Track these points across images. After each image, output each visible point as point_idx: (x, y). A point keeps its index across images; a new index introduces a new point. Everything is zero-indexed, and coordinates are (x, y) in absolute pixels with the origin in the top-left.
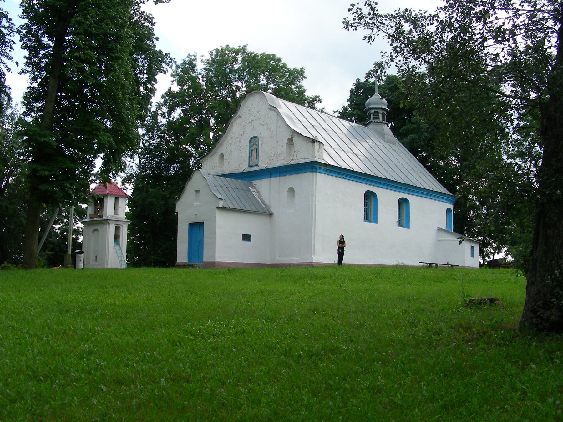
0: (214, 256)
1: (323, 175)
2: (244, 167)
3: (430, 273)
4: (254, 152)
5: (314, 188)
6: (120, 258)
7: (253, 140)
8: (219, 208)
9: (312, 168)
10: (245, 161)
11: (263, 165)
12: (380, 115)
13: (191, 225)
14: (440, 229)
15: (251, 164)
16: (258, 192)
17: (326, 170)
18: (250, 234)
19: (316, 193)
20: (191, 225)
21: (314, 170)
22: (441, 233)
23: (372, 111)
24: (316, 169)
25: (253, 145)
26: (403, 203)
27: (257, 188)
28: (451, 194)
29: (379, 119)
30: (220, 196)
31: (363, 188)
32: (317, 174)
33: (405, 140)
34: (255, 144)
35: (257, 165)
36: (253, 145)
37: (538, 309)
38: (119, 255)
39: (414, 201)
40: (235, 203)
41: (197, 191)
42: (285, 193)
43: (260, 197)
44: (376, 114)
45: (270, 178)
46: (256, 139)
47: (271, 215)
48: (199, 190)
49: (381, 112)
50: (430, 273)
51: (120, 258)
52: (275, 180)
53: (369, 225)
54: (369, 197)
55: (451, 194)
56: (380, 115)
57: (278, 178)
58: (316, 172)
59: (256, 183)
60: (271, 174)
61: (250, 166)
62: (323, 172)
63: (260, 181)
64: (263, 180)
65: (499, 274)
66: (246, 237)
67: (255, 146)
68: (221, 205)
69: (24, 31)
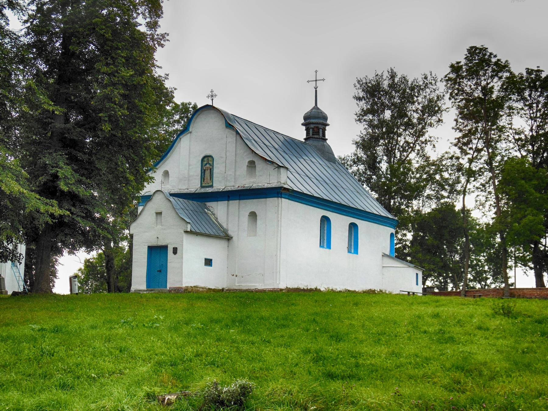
0: (181, 282)
1: (287, 200)
2: (194, 186)
4: (208, 173)
5: (280, 213)
6: (17, 278)
7: (206, 159)
8: (186, 232)
9: (278, 193)
11: (219, 186)
13: (151, 249)
14: (384, 255)
15: (204, 185)
16: (214, 215)
17: (290, 195)
18: (146, 250)
19: (281, 218)
20: (151, 249)
21: (280, 195)
22: (387, 260)
24: (281, 194)
25: (206, 164)
26: (353, 227)
27: (212, 210)
28: (390, 216)
29: (319, 135)
30: (188, 220)
31: (319, 213)
32: (283, 199)
34: (208, 163)
36: (206, 164)
38: (17, 274)
39: (362, 224)
40: (200, 229)
42: (245, 218)
43: (217, 219)
45: (228, 200)
46: (210, 159)
47: (228, 238)
51: (17, 278)
52: (234, 204)
53: (325, 251)
54: (325, 220)
55: (390, 216)
57: (238, 201)
58: (281, 197)
60: (229, 197)
61: (202, 187)
62: (287, 197)
63: (216, 203)
64: (219, 202)
66: (208, 262)
67: (208, 166)
68: (189, 230)
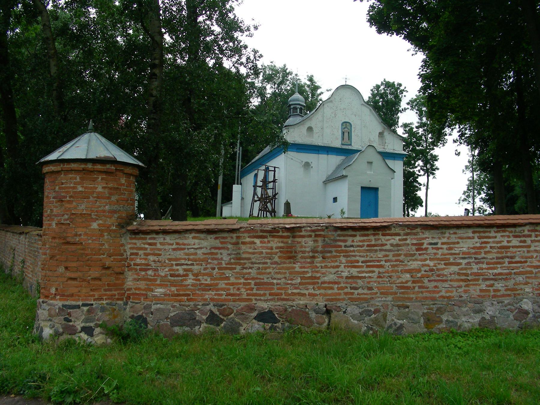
3: (80, 192)
4: (346, 135)
10: (337, 139)
12: (298, 109)
23: (292, 107)
32: (320, 155)
33: (103, 133)
35: (351, 145)
37: (68, 222)
41: (370, 163)
44: (295, 109)
48: (372, 162)
49: (299, 107)
50: (80, 192)
56: (298, 109)
57: (335, 156)
59: (86, 145)
61: (342, 144)
65: (270, 273)
69: (264, 67)
